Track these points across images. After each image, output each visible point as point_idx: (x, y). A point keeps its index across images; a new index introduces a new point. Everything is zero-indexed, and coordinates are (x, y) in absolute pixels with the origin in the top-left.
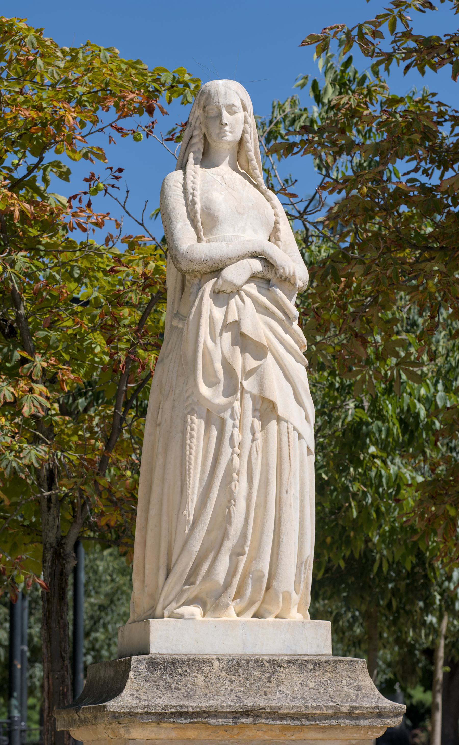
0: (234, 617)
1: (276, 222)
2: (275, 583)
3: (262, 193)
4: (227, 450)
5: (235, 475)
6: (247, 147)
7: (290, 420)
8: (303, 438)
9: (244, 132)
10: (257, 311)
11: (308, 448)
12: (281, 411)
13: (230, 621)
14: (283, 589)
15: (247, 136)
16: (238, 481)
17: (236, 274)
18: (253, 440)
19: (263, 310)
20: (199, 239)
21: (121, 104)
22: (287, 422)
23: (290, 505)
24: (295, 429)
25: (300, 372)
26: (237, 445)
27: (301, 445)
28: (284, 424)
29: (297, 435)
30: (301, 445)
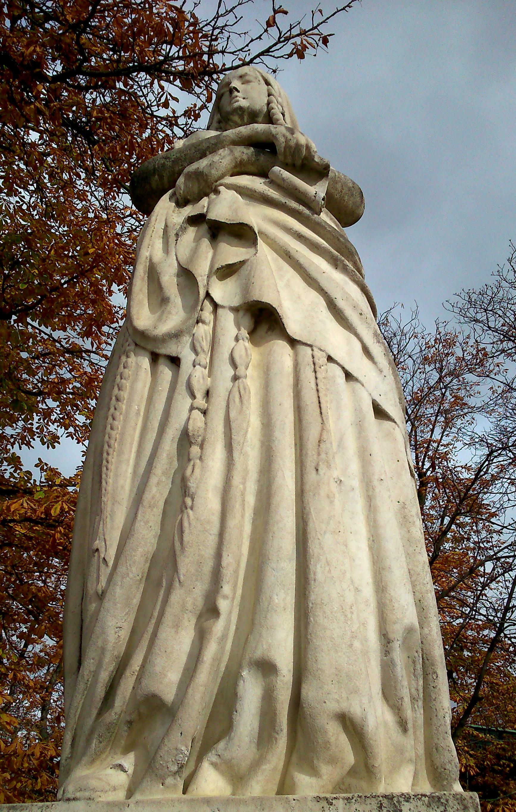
2: (309, 692)
4: (183, 403)
12: (293, 327)
14: (332, 706)
16: (201, 458)
18: (236, 378)
26: (199, 395)
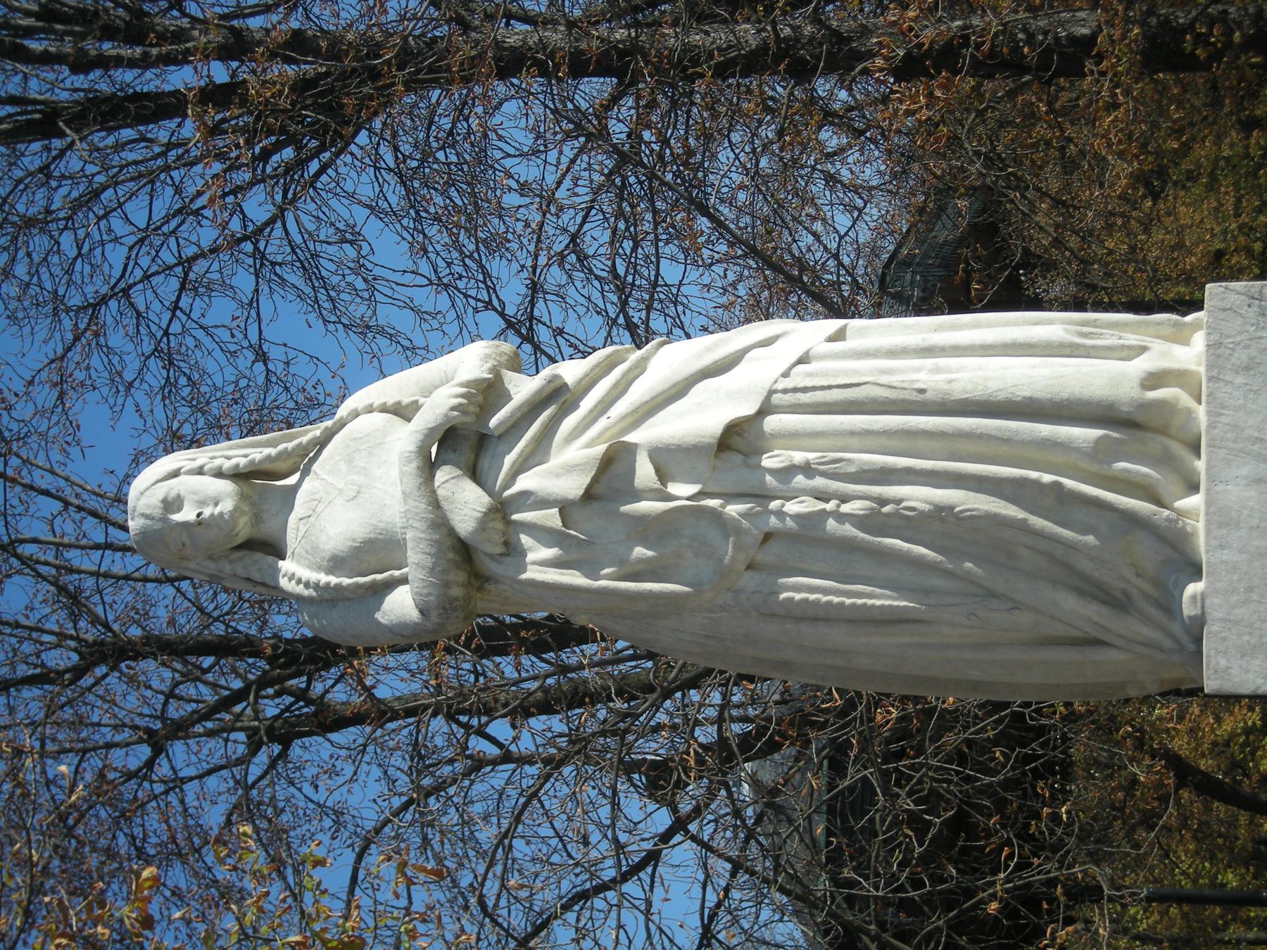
0: (1194, 502)
1: (384, 409)
3: (343, 425)
5: (886, 509)
6: (245, 466)
7: (767, 386)
8: (807, 353)
9: (219, 474)
10: (547, 461)
11: (831, 339)
12: (748, 408)
13: (1207, 514)
15: (227, 465)
17: (466, 502)
19: (538, 453)
20: (404, 581)
21: (664, 237)
22: (771, 392)
23: (950, 382)
24: (786, 375)
25: (671, 359)
26: (821, 506)
27: (822, 357)
28: (777, 399)
29: (801, 367)
30: (822, 357)
